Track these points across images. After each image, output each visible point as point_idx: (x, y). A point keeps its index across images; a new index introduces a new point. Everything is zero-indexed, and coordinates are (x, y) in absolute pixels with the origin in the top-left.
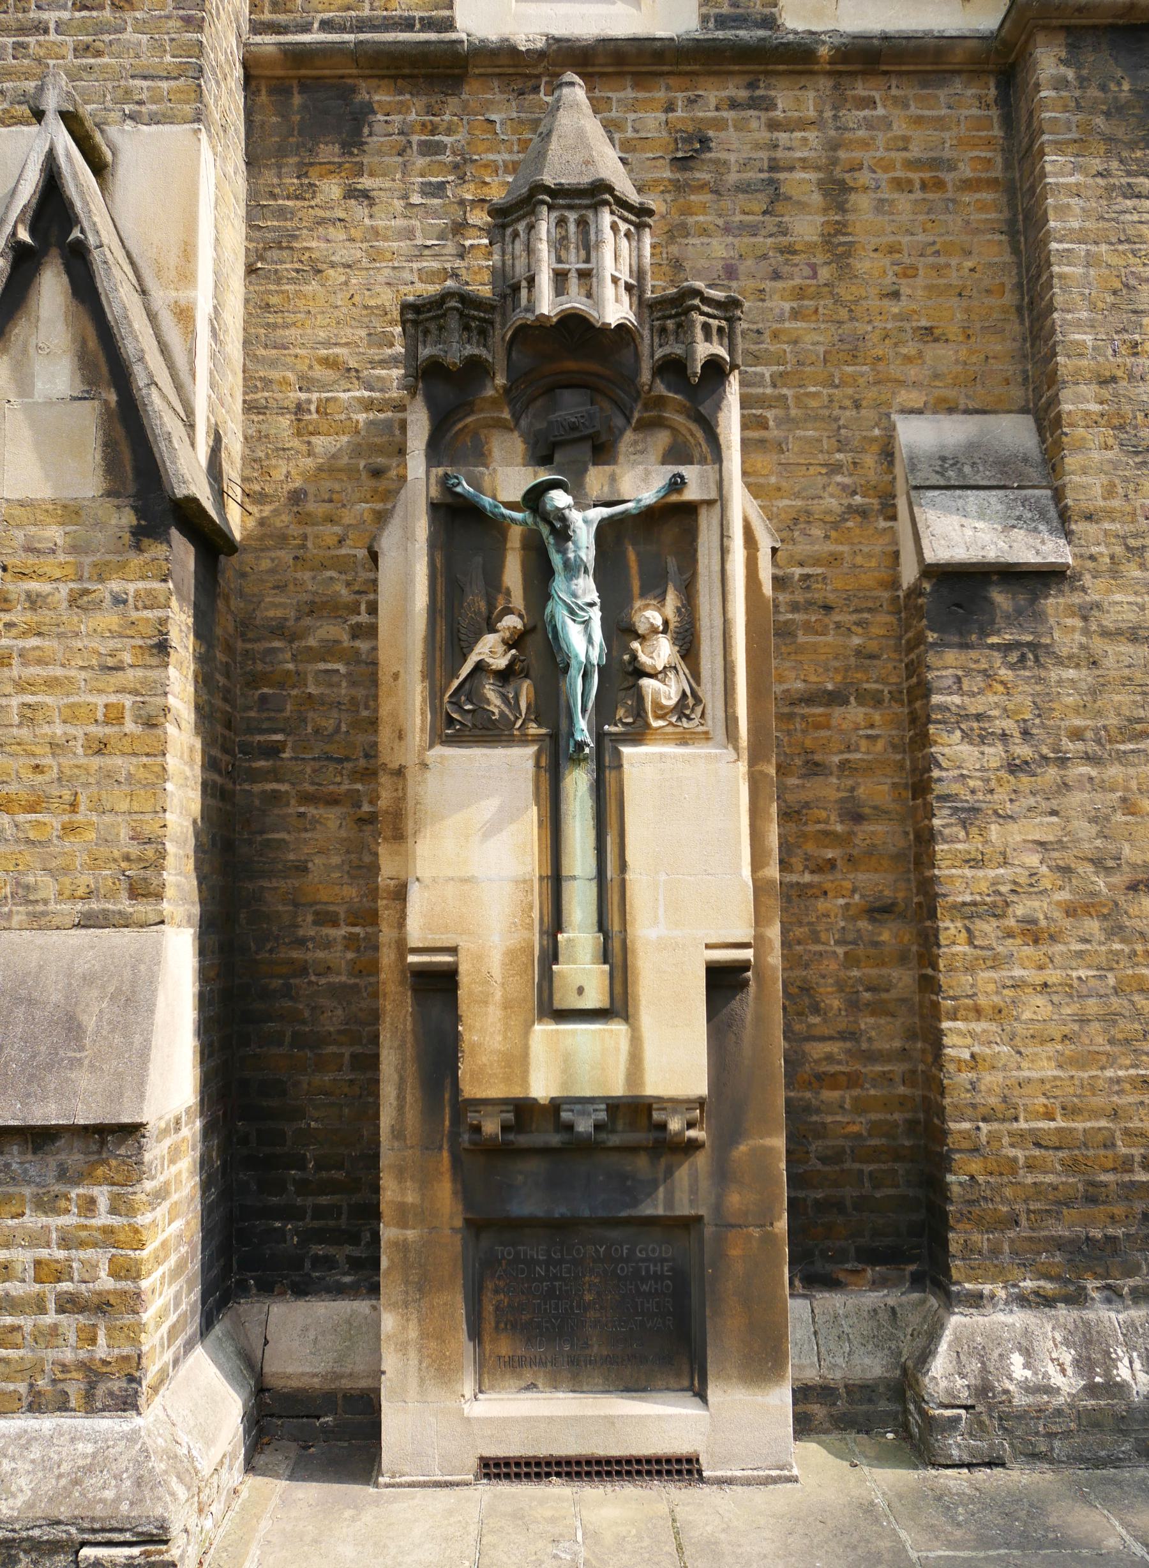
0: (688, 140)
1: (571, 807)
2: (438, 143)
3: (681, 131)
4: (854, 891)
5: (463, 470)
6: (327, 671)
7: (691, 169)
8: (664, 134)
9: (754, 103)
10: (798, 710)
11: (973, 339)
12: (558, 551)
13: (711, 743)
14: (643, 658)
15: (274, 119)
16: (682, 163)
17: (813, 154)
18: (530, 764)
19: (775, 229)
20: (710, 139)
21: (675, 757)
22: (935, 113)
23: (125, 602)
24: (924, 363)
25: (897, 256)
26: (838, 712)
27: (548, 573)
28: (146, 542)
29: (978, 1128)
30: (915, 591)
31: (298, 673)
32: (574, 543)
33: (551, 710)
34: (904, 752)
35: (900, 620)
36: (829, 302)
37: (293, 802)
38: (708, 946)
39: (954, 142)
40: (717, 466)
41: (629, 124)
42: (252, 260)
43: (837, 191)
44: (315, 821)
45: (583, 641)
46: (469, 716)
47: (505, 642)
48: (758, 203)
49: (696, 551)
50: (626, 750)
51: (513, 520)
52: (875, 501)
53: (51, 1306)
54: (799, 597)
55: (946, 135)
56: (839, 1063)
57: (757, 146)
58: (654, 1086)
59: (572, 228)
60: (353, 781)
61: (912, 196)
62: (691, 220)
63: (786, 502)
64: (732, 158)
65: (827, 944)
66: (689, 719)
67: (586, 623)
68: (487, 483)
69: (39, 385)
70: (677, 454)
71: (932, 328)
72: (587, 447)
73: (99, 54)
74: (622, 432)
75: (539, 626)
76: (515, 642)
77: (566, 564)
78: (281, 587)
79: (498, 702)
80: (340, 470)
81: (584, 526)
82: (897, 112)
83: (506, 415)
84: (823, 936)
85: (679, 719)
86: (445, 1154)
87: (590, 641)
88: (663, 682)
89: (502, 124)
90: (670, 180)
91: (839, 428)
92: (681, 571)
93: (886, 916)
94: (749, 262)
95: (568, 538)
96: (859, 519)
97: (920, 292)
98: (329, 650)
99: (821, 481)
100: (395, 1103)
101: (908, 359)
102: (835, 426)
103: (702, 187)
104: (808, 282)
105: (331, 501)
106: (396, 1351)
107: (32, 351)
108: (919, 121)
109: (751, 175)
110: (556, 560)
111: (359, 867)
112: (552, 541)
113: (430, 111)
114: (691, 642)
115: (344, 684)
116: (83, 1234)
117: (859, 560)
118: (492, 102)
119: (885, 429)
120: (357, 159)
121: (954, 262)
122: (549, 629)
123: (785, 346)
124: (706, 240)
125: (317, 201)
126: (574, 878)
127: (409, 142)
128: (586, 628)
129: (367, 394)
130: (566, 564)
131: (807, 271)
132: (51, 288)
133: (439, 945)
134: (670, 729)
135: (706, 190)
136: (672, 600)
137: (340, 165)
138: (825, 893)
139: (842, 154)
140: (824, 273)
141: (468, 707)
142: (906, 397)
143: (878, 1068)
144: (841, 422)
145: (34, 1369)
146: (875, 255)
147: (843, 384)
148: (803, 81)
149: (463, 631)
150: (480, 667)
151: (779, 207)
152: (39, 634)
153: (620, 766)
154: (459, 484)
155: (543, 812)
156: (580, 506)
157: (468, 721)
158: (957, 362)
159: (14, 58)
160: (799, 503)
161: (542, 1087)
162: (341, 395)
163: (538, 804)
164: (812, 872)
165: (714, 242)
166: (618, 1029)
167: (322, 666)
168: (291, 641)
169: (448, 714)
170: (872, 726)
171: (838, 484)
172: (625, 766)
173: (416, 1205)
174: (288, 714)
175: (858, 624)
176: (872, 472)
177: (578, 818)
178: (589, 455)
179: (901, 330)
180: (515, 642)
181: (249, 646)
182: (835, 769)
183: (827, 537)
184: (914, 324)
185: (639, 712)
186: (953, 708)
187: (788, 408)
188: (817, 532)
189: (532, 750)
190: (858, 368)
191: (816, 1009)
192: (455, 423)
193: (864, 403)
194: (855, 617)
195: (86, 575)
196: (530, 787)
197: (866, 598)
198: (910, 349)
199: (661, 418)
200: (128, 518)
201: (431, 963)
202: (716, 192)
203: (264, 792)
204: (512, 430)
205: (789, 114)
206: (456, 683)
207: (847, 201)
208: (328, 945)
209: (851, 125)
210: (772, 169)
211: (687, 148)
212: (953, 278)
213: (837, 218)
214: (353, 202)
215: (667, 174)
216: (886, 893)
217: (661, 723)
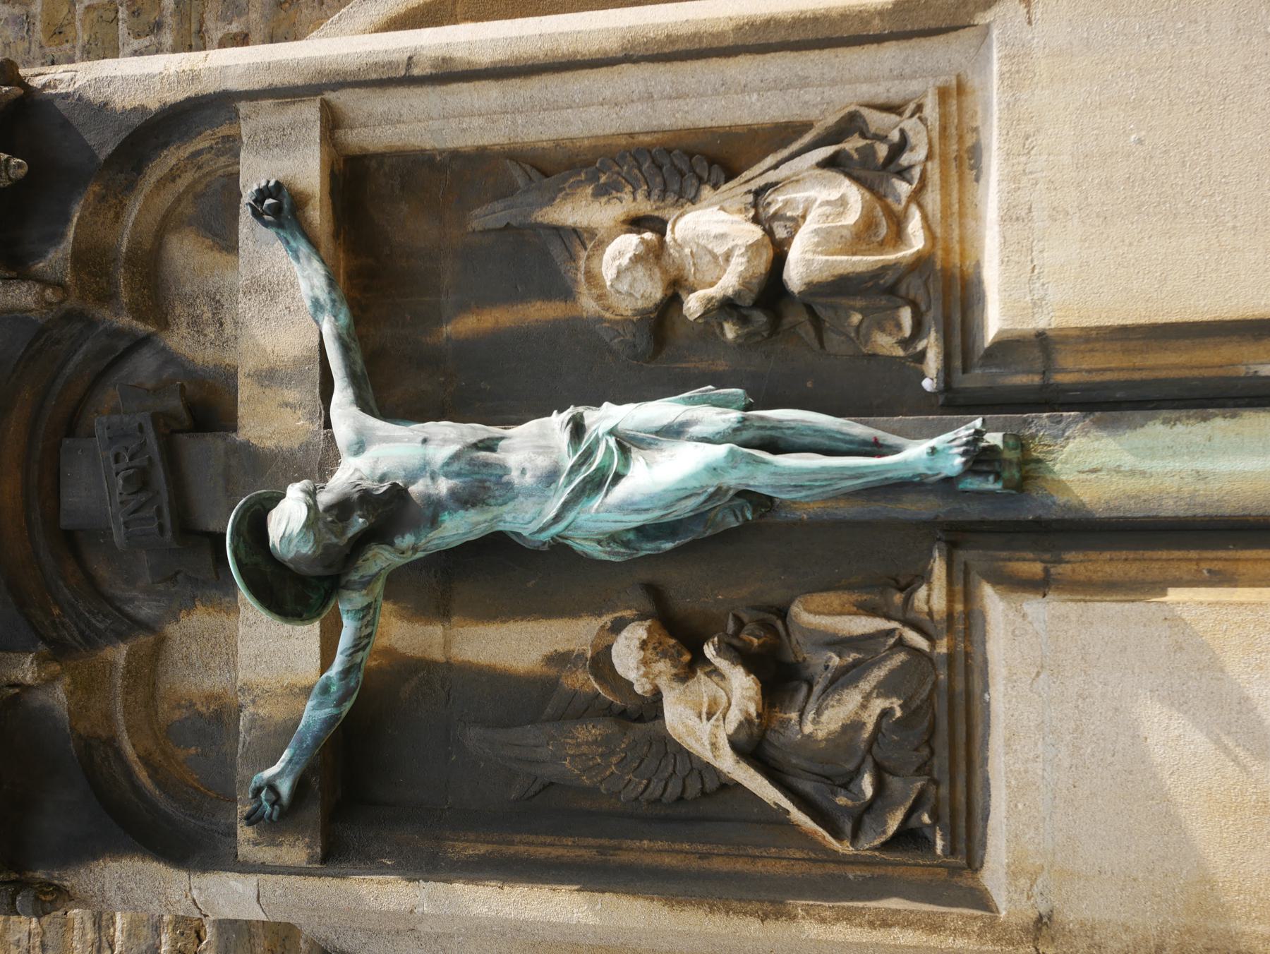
1: (1171, 484)
5: (242, 771)
12: (434, 522)
13: (973, 81)
14: (728, 282)
18: (1037, 608)
21: (1013, 179)
27: (497, 549)
32: (413, 478)
33: (879, 542)
40: (243, 107)
45: (675, 451)
46: (895, 783)
47: (685, 675)
49: (456, 155)
50: (995, 322)
51: (359, 645)
67: (626, 444)
68: (271, 711)
74: (170, 358)
75: (645, 575)
76: (684, 640)
77: (467, 499)
79: (852, 699)
81: (372, 452)
83: (119, 654)
85: (903, 173)
87: (674, 432)
88: (796, 223)
92: (506, 192)
95: (398, 494)
100: (385, 77)
110: (458, 527)
112: (407, 540)
122: (648, 548)
128: (641, 443)
130: (467, 499)
134: (933, 198)
136: (579, 210)
141: (867, 785)
149: (656, 789)
153: (1044, 342)
154: (271, 786)
155: (1185, 570)
156: (322, 461)
157: (906, 788)
163: (1160, 586)
169: (887, 846)
172: (1041, 322)
177: (1203, 465)
178: (213, 443)
180: (684, 640)
185: (881, 289)
189: (993, 601)
192: (136, 788)
196: (1107, 610)
199: (133, 259)
204: (162, 641)
217: (915, 226)
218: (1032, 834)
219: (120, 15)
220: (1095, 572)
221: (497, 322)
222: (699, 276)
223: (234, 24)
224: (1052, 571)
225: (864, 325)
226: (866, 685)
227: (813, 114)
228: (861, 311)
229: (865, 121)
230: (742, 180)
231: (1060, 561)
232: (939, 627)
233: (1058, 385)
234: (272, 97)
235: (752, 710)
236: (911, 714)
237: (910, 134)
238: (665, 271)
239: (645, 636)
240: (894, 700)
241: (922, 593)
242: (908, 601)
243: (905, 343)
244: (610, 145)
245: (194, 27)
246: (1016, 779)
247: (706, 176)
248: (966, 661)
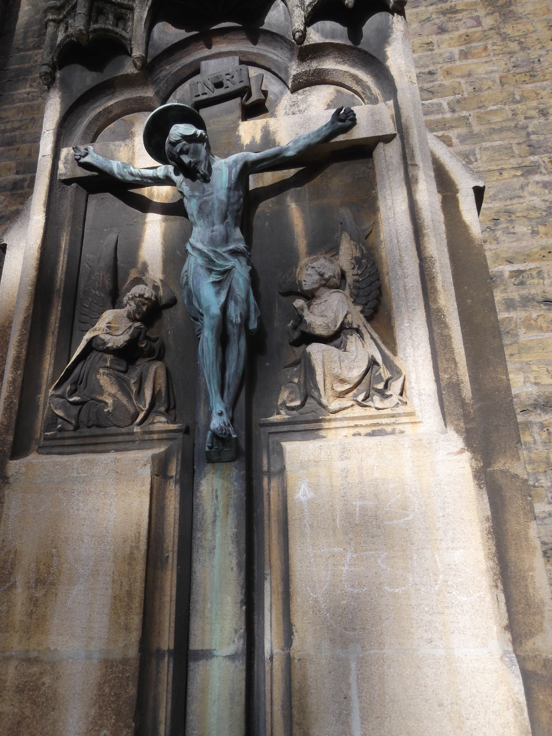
91: (528, 134)
100: (407, 155)
102: (524, 133)
134: (358, 411)
171: (538, 183)
183: (534, 233)
187: (469, 125)
188: (522, 229)
190: (539, 84)
218: (45, 473)
219: (457, 96)
220: (170, 501)
221: (296, 225)
222: (316, 306)
223: (456, 140)
224: (172, 480)
225: (293, 384)
226: (119, 395)
227: (400, 354)
228: (299, 381)
229: (397, 379)
230: (366, 324)
231: (176, 484)
232: (146, 427)
233: (262, 479)
234: (395, 112)
235: (109, 345)
237: (390, 399)
238: (318, 289)
239: (146, 296)
240: (112, 408)
241: (163, 419)
242: (161, 414)
243: (284, 403)
244: (383, 265)
245: (453, 125)
246: (70, 464)
247: (367, 307)
248: (131, 441)
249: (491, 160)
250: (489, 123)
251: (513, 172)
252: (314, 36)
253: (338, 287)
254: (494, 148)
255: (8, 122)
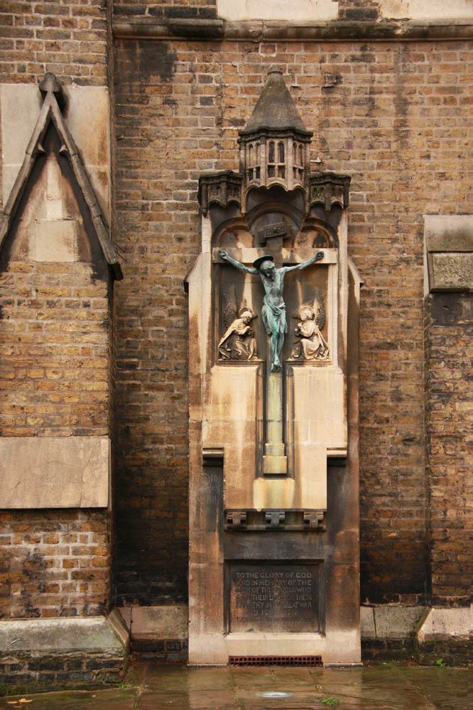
0: (331, 78)
2: (209, 77)
3: (328, 73)
4: (397, 432)
6: (157, 331)
7: (332, 93)
8: (320, 74)
9: (364, 58)
10: (373, 351)
11: (464, 179)
15: (127, 61)
16: (328, 90)
17: (392, 85)
19: (371, 124)
20: (341, 77)
22: (453, 63)
23: (89, 306)
24: (440, 190)
25: (429, 137)
26: (392, 353)
28: (97, 281)
29: (446, 531)
30: (428, 300)
31: (144, 331)
34: (422, 371)
35: (422, 311)
36: (396, 160)
37: (142, 389)
38: (328, 449)
39: (462, 79)
41: (302, 68)
42: (118, 134)
43: (402, 106)
44: (153, 398)
48: (364, 110)
50: (295, 369)
52: (414, 256)
53: (70, 576)
54: (376, 300)
55: (458, 75)
56: (388, 506)
57: (365, 81)
58: (305, 505)
59: (276, 147)
60: (170, 380)
61: (439, 107)
62: (331, 119)
63: (371, 256)
64: (352, 87)
65: (384, 455)
66: (322, 356)
69: (49, 213)
70: (320, 242)
71: (444, 173)
72: (281, 240)
73: (59, 48)
78: (136, 292)
79: (242, 348)
80: (162, 238)
82: (434, 62)
84: (382, 451)
86: (217, 534)
89: (240, 67)
90: (321, 98)
91: (398, 221)
93: (411, 443)
94: (358, 140)
96: (405, 265)
97: (440, 155)
98: (158, 321)
99: (388, 246)
101: (433, 188)
102: (396, 220)
103: (337, 102)
104: (386, 150)
105: (158, 252)
106: (195, 613)
107: (45, 198)
108: (445, 67)
109: (360, 96)
111: (173, 418)
113: (204, 59)
114: (324, 324)
115: (165, 336)
116: (83, 550)
117: (404, 284)
118: (235, 56)
119: (420, 222)
120: (169, 84)
121: (457, 140)
122: (264, 317)
123: (374, 182)
124: (338, 129)
125: (148, 106)
126: (272, 421)
127: (195, 76)
129: (175, 201)
131: (386, 145)
132: (52, 171)
133: (216, 447)
134: (315, 360)
135: (339, 103)
136: (316, 305)
137: (161, 86)
138: (384, 432)
139: (406, 85)
140: (394, 146)
141: (229, 350)
142: (431, 207)
143: (405, 509)
144: (399, 218)
145: (64, 600)
146: (419, 137)
147: (400, 200)
148: (389, 46)
150: (234, 333)
151: (374, 113)
152: (52, 318)
158: (456, 189)
159: (17, 48)
160: (377, 257)
161: (259, 505)
162: (163, 202)
164: (378, 423)
165: (342, 130)
166: (290, 482)
167: (155, 328)
168: (141, 317)
170: (408, 359)
171: (396, 248)
173: (206, 554)
174: (139, 349)
175: (403, 313)
176: (412, 242)
179: (430, 174)
180: (249, 322)
181: (121, 318)
182: (390, 378)
183: (390, 272)
184: (437, 171)
185: (301, 352)
186: (441, 352)
187: (374, 212)
188: (385, 270)
189: (255, 368)
190: (409, 193)
191: (378, 482)
193: (410, 210)
194: (401, 309)
195: (72, 294)
197: (407, 301)
198: (433, 183)
200: (90, 271)
201: (212, 454)
202: (344, 105)
203: (129, 384)
205: (381, 64)
206: (223, 340)
207: (407, 109)
208: (158, 451)
209: (412, 70)
210: (371, 93)
211: (330, 82)
212: (457, 149)
213: (402, 118)
214: (167, 106)
215: (320, 95)
216: (412, 433)
236: (239, 356)
249: (379, 233)
250: (383, 211)
251: (387, 241)
252: (313, 215)
253: (312, 319)
254: (382, 226)
255: (131, 160)
